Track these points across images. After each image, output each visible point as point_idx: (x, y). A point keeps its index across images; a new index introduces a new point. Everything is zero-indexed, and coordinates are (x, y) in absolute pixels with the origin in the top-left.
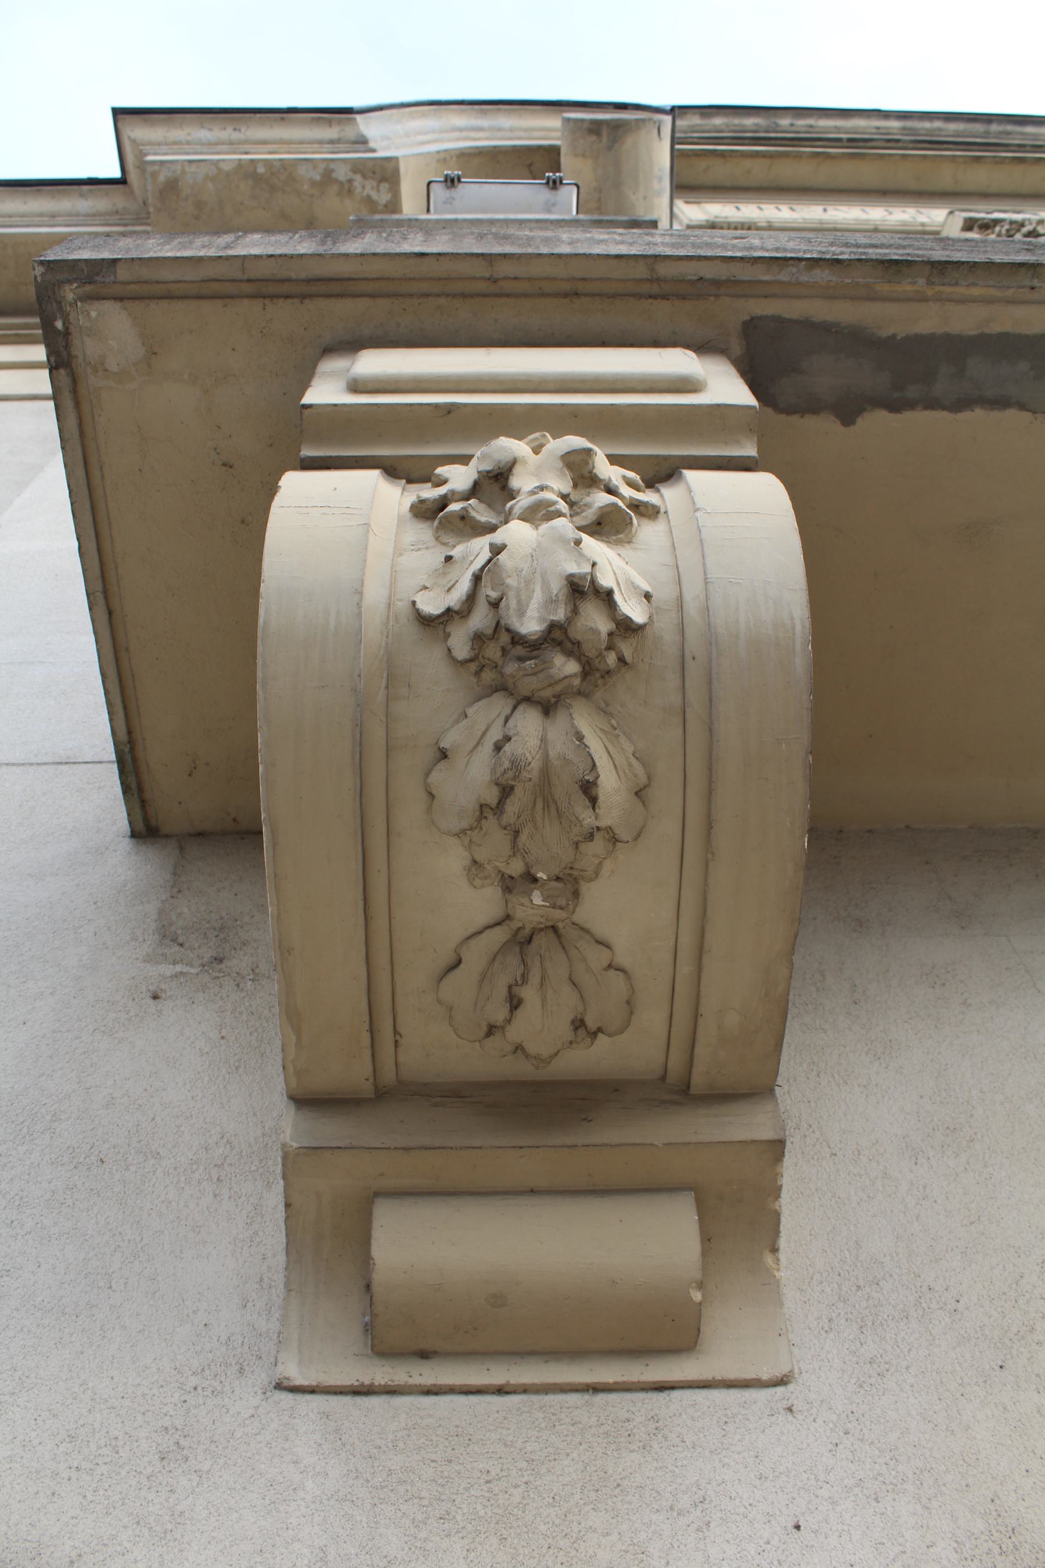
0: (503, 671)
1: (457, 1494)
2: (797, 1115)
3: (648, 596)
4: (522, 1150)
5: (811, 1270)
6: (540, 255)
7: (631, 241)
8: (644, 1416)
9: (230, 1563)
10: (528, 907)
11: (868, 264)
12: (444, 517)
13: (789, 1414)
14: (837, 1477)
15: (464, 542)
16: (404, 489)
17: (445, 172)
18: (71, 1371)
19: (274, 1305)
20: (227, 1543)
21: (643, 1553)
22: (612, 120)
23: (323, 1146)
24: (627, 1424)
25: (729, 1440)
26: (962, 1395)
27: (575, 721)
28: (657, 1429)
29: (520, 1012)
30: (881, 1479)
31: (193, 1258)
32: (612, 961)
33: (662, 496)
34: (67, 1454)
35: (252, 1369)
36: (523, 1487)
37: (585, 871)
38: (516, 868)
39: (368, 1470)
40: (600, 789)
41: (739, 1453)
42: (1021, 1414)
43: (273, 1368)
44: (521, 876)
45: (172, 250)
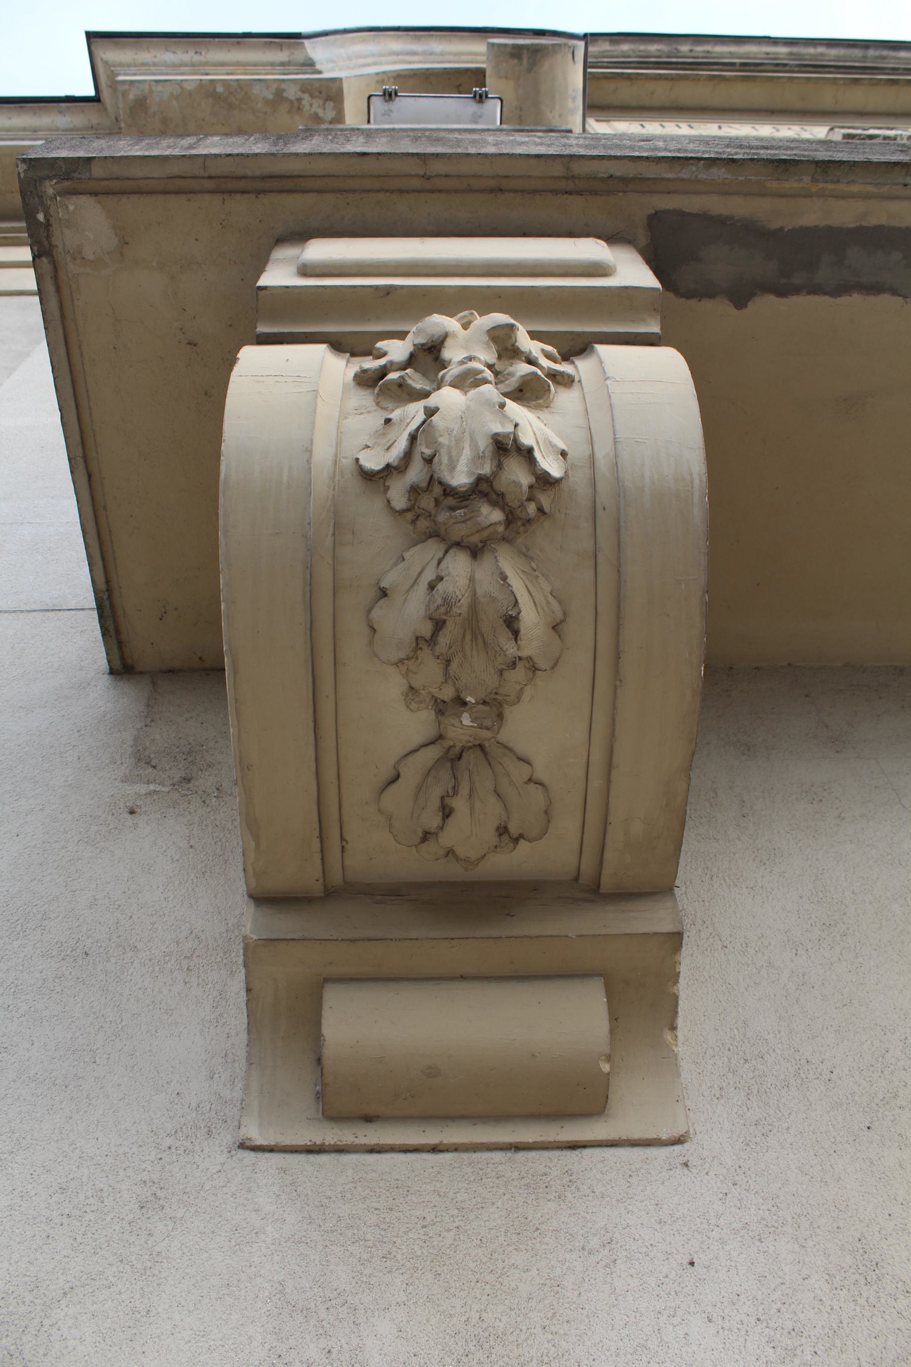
0: (436, 519)
1: (398, 1237)
2: (693, 913)
3: (564, 454)
4: (452, 941)
5: (705, 1046)
6: (468, 155)
7: (549, 143)
8: (559, 1171)
9: (202, 1294)
10: (458, 727)
11: (759, 163)
12: (383, 384)
13: (685, 1168)
14: (726, 1221)
15: (401, 407)
16: (348, 362)
17: (384, 87)
18: (61, 1133)
19: (237, 1077)
20: (198, 1278)
21: (558, 1286)
22: (532, 45)
23: (280, 938)
24: (544, 1177)
25: (634, 1190)
26: (835, 1152)
27: (500, 564)
28: (570, 1181)
29: (451, 821)
30: (764, 1223)
31: (167, 1037)
32: (532, 775)
33: (576, 367)
34: (59, 1203)
35: (218, 1131)
36: (454, 1230)
37: (509, 696)
38: (447, 693)
39: (320, 1217)
40: (521, 623)
41: (642, 1202)
42: (885, 1167)
43: (237, 1130)
44: (452, 700)
45: (140, 150)
